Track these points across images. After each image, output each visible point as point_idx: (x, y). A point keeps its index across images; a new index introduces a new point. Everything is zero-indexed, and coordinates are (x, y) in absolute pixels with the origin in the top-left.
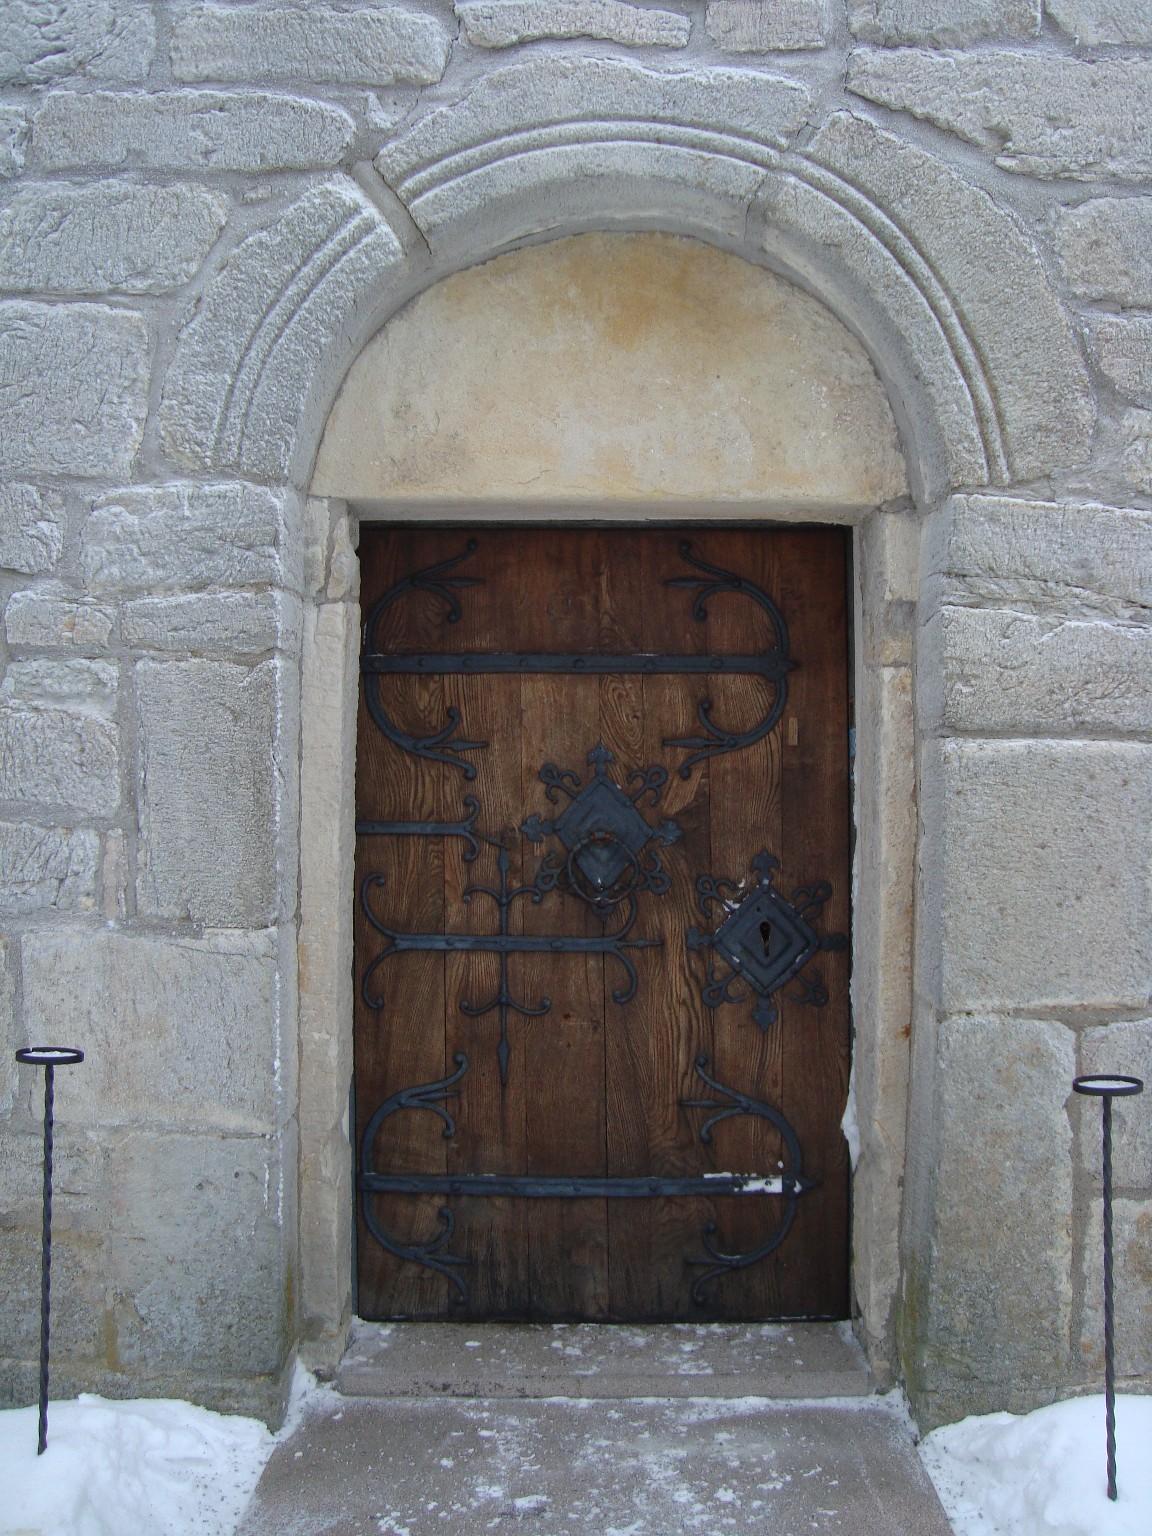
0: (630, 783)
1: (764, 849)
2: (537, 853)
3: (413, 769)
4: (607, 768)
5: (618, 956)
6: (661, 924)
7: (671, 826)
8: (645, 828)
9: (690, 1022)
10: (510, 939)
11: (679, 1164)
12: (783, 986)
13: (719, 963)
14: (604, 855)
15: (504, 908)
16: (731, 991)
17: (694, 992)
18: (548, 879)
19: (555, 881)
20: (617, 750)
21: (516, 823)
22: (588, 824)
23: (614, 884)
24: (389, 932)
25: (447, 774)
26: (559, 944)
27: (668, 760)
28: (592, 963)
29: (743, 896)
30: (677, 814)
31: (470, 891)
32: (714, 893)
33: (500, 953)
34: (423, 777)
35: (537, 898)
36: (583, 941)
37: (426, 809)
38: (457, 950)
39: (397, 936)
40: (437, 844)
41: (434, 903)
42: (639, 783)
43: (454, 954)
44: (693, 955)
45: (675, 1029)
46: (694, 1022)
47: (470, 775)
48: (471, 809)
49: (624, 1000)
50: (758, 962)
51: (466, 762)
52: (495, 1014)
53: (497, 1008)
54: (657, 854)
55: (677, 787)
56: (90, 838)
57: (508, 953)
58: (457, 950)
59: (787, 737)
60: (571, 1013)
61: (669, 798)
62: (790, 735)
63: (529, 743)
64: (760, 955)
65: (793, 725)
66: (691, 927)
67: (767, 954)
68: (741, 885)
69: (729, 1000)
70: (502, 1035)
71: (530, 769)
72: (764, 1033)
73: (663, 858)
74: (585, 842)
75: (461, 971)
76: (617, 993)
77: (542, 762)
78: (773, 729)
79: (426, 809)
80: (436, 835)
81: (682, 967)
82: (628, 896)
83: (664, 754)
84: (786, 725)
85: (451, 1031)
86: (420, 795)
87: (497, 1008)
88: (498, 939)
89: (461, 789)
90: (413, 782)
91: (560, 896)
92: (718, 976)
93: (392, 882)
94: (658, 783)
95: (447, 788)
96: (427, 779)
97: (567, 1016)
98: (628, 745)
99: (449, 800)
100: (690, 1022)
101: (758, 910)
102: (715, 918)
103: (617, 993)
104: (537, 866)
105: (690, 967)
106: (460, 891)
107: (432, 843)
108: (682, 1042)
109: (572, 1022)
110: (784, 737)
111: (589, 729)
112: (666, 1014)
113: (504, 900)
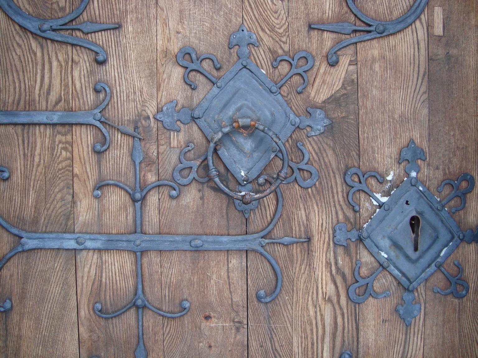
0: (275, 68)
1: (412, 141)
2: (174, 143)
3: (39, 54)
4: (250, 52)
5: (261, 254)
6: (308, 219)
7: (319, 114)
8: (292, 116)
9: (335, 318)
10: (145, 237)
11: (214, 15)
12: (426, 280)
13: (366, 257)
14: (248, 144)
15: (138, 204)
16: (377, 286)
17: (340, 288)
18: (186, 172)
19: (193, 175)
20: (261, 33)
21: (151, 110)
22: (230, 112)
23: (259, 176)
24: (15, 231)
25: (76, 58)
26: (198, 242)
27: (315, 46)
28: (235, 262)
29: (391, 189)
30: (324, 102)
31: (101, 186)
32: (363, 187)
33: (135, 253)
34: (50, 63)
35: (174, 193)
36: (225, 239)
37: (53, 97)
38: (85, 249)
39: (23, 234)
40: (65, 134)
41: (62, 199)
42: (284, 68)
43: (84, 253)
44: (340, 251)
45: (320, 327)
46: (339, 319)
47: (101, 58)
48: (102, 96)
49: (268, 299)
50: (407, 257)
51: (96, 44)
52: (132, 313)
53: (133, 311)
54: (303, 145)
55: (325, 73)
56: (113, 232)
57: (143, 252)
58: (85, 249)
59: (433, 27)
60: (212, 315)
61: (316, 85)
62: (436, 25)
63: (165, 23)
64: (410, 251)
65: (438, 14)
66: (338, 222)
67: (416, 249)
68: (389, 178)
69: (375, 295)
70: (140, 338)
71: (166, 53)
72: (408, 326)
73: (309, 148)
74: (226, 130)
75: (93, 272)
76: (262, 292)
77: (180, 45)
78: (418, 17)
79: (53, 97)
80: (63, 125)
81: (328, 264)
82: (275, 191)
83: (310, 38)
84: (431, 15)
85: (85, 334)
86: (47, 80)
87: (133, 311)
88: (131, 237)
89: (91, 73)
90: (39, 67)
91: (200, 191)
92: (364, 271)
93: (17, 178)
94: (306, 68)
95: (76, 74)
96: (55, 64)
97: (208, 318)
98: (272, 30)
99: (78, 86)
100: (335, 318)
101: (407, 203)
102: (364, 213)
103: (262, 292)
104: (174, 158)
105: (336, 263)
106: (91, 184)
107: (59, 133)
108: (327, 339)
109: (213, 323)
110: (430, 26)
111: (231, 10)
112: (312, 313)
113: (138, 196)
